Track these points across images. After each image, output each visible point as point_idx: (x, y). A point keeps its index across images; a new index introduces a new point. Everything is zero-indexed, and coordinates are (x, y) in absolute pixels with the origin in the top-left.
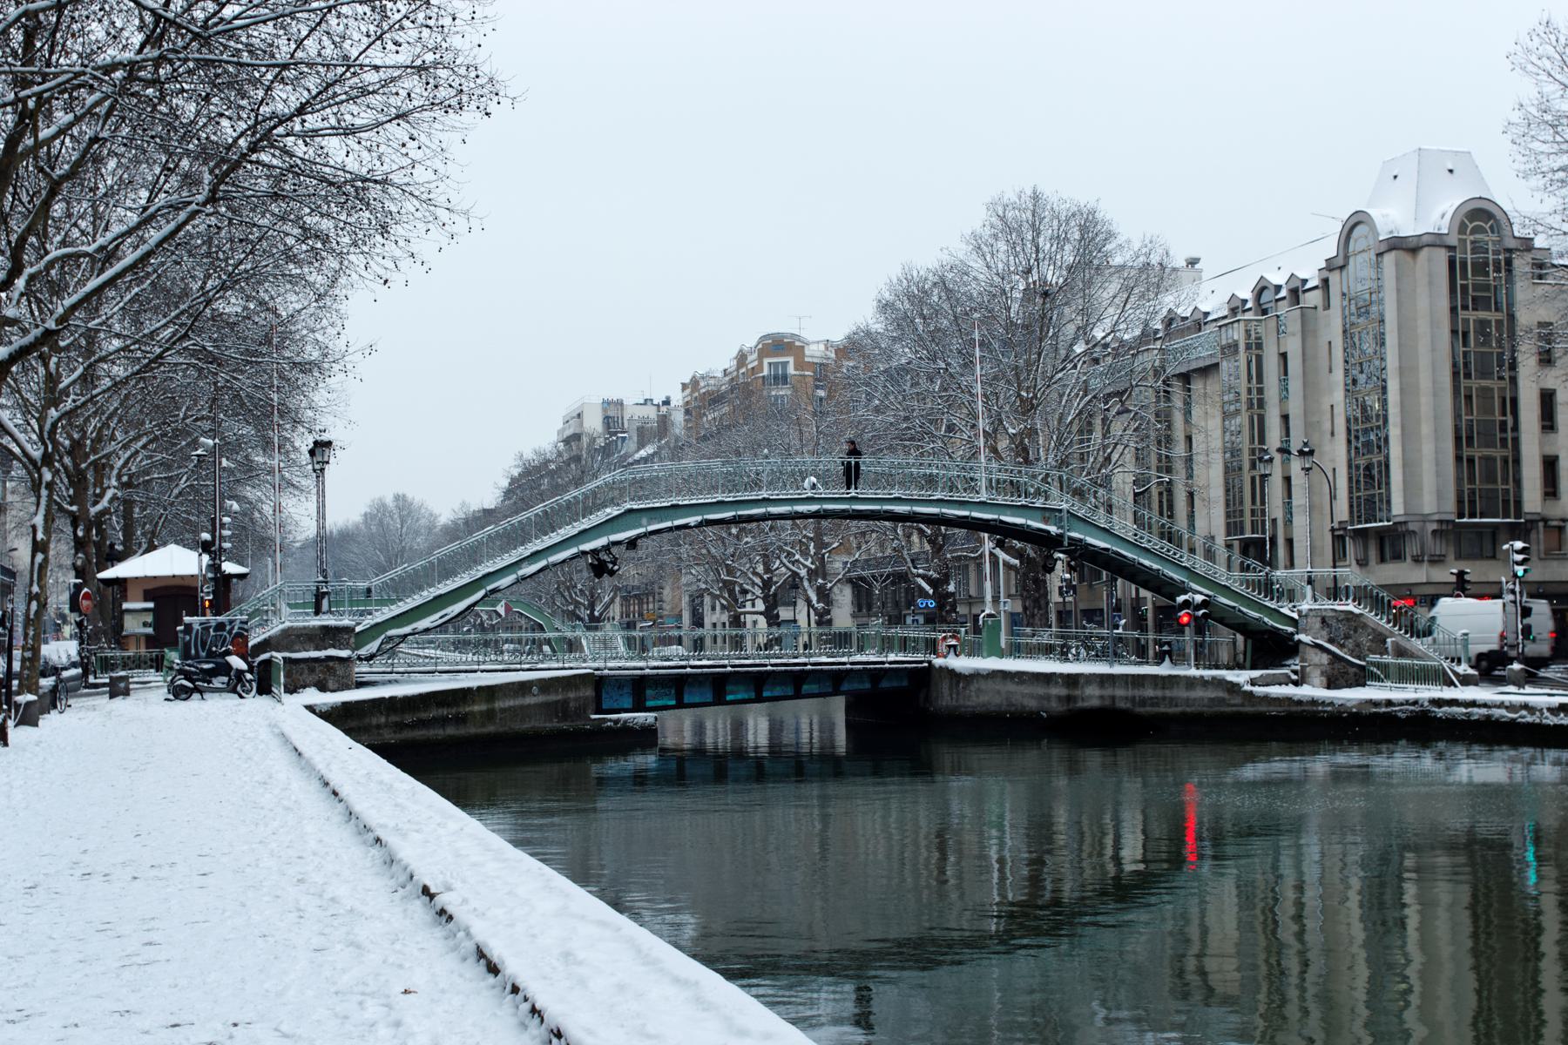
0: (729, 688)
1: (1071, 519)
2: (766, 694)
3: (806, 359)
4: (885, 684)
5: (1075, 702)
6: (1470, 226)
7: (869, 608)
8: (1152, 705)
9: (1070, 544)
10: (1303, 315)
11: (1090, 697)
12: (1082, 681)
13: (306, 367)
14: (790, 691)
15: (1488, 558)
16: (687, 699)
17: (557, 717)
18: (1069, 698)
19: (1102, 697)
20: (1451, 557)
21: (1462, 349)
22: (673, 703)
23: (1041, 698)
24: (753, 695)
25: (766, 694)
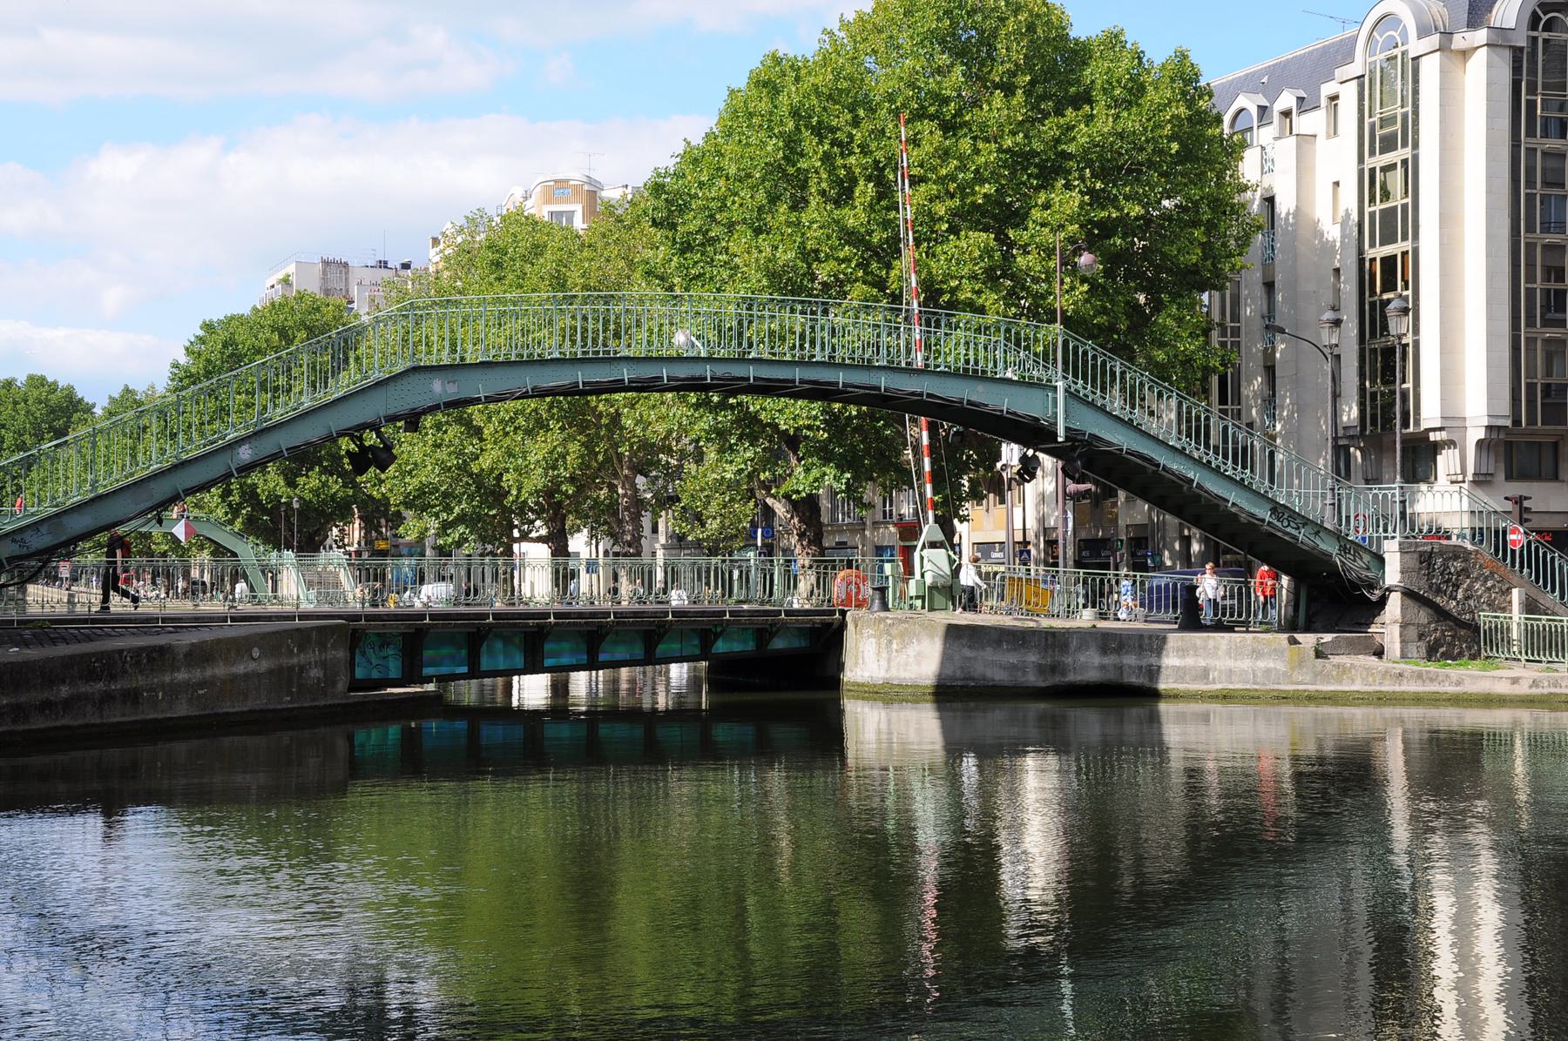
0: (548, 647)
1: (1071, 401)
2: (602, 657)
3: (516, 678)
4: (779, 644)
5: (1063, 674)
6: (1545, 18)
7: (1348, 476)
8: (1195, 679)
9: (1067, 438)
10: (1299, 147)
11: (1084, 667)
12: (1074, 643)
13: (1021, 825)
14: (638, 651)
15: (1550, 480)
16: (485, 664)
17: (290, 693)
18: (1054, 669)
19: (1103, 667)
20: (1501, 476)
21: (363, 622)
22: (464, 669)
23: (1013, 667)
24: (584, 658)
25: (602, 657)
